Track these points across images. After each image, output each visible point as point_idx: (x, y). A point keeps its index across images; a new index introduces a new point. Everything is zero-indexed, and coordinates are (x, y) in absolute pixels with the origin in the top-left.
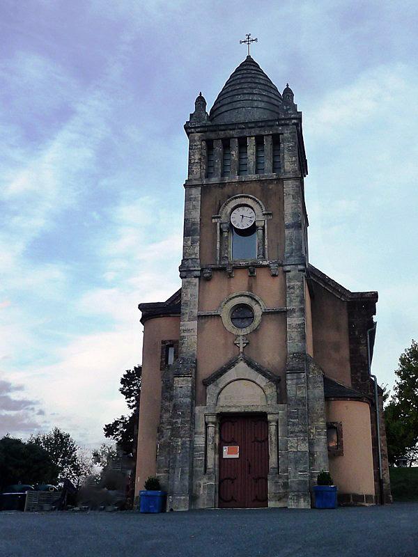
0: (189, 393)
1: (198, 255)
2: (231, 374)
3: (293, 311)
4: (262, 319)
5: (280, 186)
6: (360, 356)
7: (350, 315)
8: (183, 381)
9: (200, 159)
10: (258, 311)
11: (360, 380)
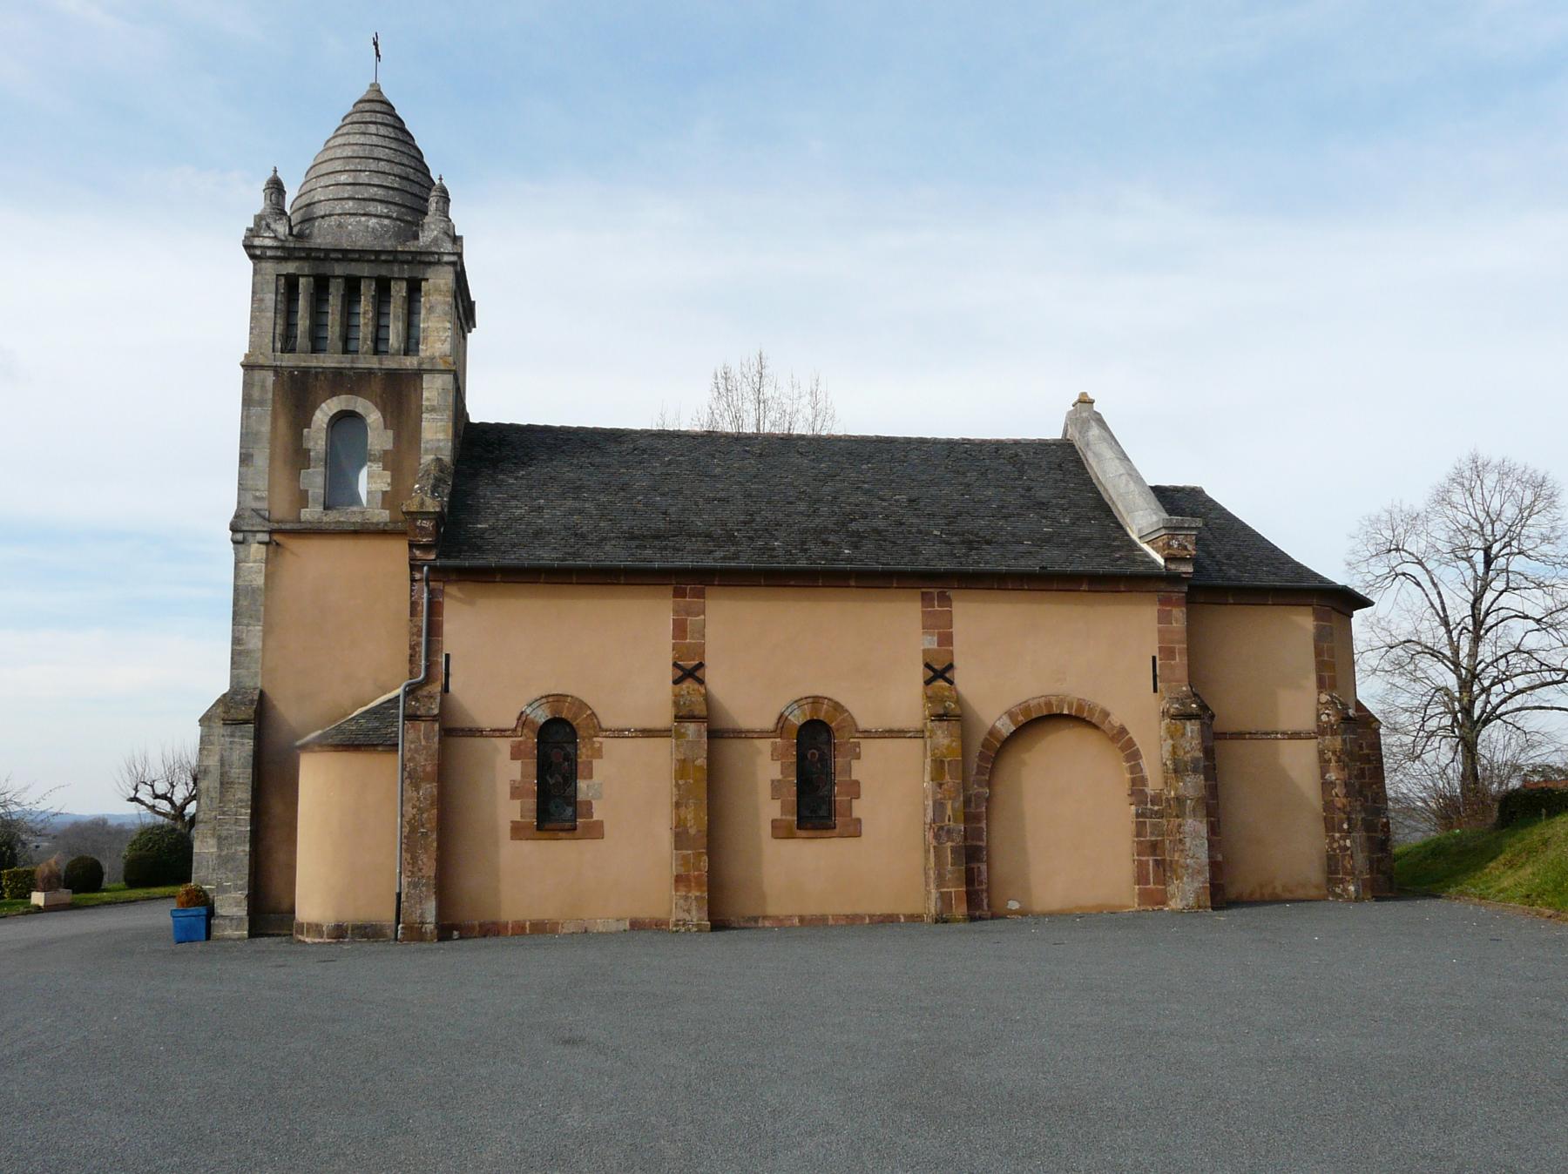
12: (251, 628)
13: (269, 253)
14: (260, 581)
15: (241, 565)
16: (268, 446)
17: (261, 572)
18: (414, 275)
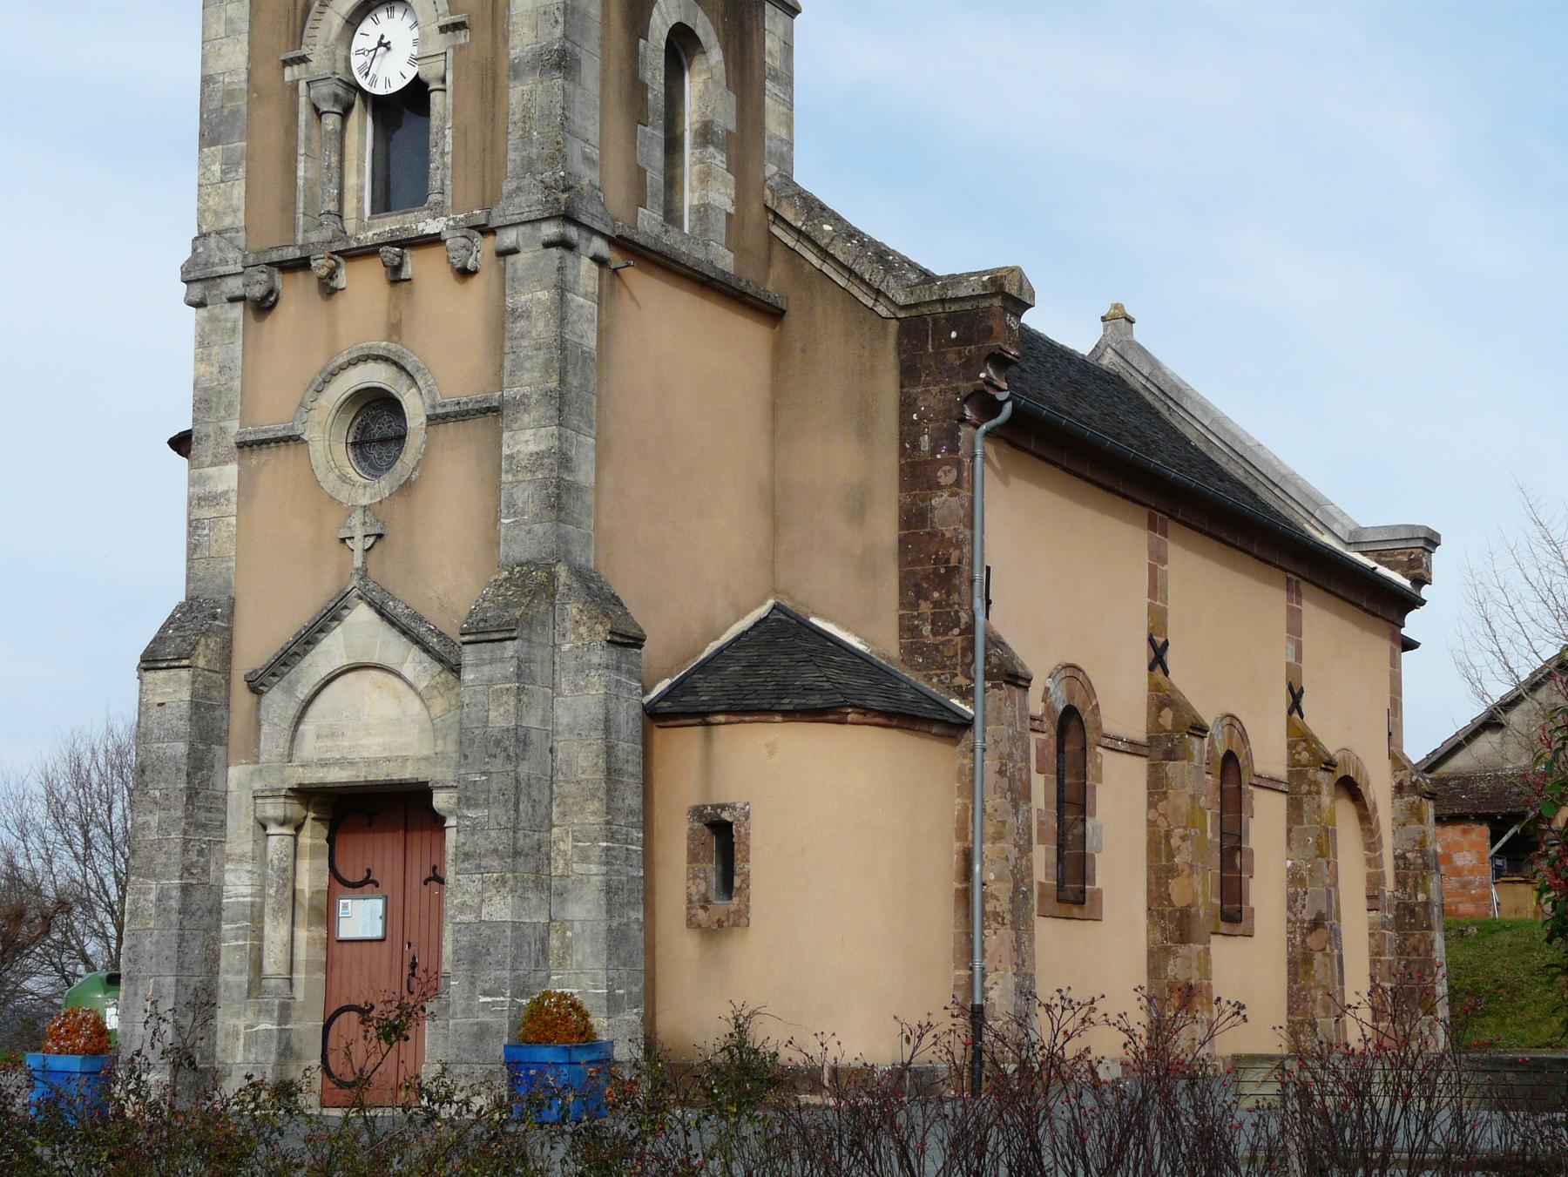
0: (184, 727)
1: (241, 215)
2: (332, 651)
3: (520, 403)
4: (429, 444)
6: (932, 535)
7: (909, 373)
8: (166, 681)
10: (415, 408)
11: (926, 629)
12: (582, 438)
14: (591, 341)
15: (569, 295)
16: (598, 51)
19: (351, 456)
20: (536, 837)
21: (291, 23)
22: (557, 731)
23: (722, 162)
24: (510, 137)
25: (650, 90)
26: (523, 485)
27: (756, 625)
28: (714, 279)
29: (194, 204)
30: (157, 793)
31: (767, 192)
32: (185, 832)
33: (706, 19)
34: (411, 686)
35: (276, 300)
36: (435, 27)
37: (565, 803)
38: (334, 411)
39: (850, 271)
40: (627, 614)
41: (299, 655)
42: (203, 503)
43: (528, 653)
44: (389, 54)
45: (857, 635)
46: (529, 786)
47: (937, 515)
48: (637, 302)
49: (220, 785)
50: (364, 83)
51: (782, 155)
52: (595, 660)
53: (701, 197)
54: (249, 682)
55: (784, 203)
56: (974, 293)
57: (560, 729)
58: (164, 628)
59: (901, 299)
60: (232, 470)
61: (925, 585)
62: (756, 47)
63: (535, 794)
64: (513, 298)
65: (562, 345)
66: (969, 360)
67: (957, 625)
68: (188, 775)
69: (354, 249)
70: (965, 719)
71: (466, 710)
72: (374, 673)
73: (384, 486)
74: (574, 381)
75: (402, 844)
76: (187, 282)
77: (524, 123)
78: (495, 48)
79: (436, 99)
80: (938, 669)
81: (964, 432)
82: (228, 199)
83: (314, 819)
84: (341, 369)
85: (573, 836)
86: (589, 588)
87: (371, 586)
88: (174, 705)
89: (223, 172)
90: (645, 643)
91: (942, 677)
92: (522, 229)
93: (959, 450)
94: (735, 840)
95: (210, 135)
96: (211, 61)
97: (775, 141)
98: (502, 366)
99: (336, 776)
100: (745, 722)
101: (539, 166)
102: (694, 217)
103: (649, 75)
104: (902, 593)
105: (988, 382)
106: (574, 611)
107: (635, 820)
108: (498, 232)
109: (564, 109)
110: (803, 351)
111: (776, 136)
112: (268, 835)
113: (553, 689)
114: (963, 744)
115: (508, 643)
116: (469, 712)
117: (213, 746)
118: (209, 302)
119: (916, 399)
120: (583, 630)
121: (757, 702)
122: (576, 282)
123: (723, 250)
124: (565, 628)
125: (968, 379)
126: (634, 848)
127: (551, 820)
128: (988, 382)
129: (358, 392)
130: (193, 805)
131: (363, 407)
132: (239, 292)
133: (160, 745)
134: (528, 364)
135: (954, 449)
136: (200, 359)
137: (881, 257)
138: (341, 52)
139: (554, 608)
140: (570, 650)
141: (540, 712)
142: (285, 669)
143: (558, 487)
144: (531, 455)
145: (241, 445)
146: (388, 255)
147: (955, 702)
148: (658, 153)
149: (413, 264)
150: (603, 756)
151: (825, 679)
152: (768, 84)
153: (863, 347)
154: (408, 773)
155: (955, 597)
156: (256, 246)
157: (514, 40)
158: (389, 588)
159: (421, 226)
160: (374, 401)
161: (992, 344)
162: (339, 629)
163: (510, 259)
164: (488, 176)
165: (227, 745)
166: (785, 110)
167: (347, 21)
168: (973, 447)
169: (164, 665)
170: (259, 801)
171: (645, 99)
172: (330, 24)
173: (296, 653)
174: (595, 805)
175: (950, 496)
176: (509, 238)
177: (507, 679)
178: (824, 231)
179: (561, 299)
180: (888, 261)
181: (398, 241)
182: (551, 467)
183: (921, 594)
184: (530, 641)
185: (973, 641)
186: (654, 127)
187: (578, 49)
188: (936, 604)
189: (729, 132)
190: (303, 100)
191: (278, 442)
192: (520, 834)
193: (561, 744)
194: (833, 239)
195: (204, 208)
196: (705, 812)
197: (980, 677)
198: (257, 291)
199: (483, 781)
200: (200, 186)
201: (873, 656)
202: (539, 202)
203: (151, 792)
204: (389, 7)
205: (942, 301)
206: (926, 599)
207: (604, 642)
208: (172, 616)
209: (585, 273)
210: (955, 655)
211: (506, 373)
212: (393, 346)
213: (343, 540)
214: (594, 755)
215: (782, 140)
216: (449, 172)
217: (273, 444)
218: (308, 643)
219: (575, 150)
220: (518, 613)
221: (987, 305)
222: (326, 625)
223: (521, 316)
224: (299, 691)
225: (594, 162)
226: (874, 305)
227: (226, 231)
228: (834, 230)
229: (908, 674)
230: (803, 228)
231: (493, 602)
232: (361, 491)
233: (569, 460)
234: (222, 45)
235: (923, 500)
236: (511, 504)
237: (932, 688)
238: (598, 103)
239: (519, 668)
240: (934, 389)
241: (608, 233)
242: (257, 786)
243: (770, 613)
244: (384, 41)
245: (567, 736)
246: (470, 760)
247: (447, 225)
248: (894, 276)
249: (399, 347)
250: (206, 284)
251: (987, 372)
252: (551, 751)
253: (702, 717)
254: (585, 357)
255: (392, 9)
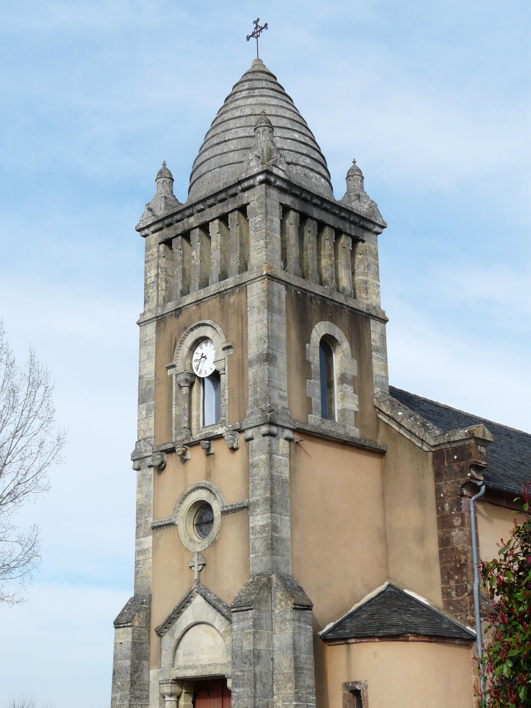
0: (129, 653)
1: (153, 431)
4: (222, 523)
5: (243, 295)
6: (453, 549)
7: (438, 476)
8: (123, 633)
9: (157, 275)
11: (454, 593)
12: (283, 517)
13: (278, 183)
14: (286, 474)
15: (274, 456)
16: (285, 351)
17: (287, 465)
18: (358, 235)
19: (195, 530)
20: (266, 701)
21: (170, 352)
22: (275, 650)
23: (351, 390)
24: (249, 391)
25: (312, 364)
26: (258, 540)
27: (379, 594)
28: (347, 441)
29: (136, 428)
30: (120, 684)
31: (375, 400)
32: (130, 701)
33: (339, 330)
34: (218, 631)
35: (165, 466)
36: (221, 348)
37: (279, 684)
38: (187, 511)
39: (411, 432)
40: (305, 595)
41: (175, 619)
42: (140, 554)
43: (259, 615)
44: (206, 360)
45: (424, 597)
46: (261, 676)
47: (455, 540)
48: (309, 455)
49: (146, 679)
50: (197, 373)
51: (382, 383)
52: (288, 617)
53: (342, 406)
54: (156, 631)
55: (382, 404)
56: (462, 438)
57: (276, 649)
58: (124, 609)
59: (432, 443)
60: (150, 538)
61: (452, 573)
62: (366, 339)
63: (265, 680)
64: (252, 459)
65: (271, 477)
66: (463, 468)
67: (467, 591)
68: (131, 675)
69: (192, 442)
70: (473, 636)
71: (234, 642)
72: (204, 626)
73: (206, 543)
74: (278, 492)
75: (221, 704)
76: (133, 460)
77: (254, 384)
78: (242, 354)
79: (222, 377)
80: (460, 612)
81: (464, 501)
82: (148, 425)
83: (185, 693)
84: (189, 493)
85: (282, 699)
86: (286, 584)
87: (201, 587)
88: (126, 643)
89: (146, 414)
90: (313, 608)
91: (462, 616)
92: (254, 429)
93: (461, 509)
94: (362, 699)
95: (142, 400)
96: (142, 371)
97: (378, 377)
98: (248, 488)
99: (190, 673)
100: (363, 642)
101: (260, 402)
102: (339, 415)
103: (311, 358)
104: (442, 577)
105: (472, 477)
106: (279, 595)
107: (311, 691)
108: (245, 431)
109: (269, 378)
110: (394, 468)
111: (378, 375)
112: (166, 701)
113: (272, 631)
114: (473, 648)
115: (250, 611)
116: (235, 643)
117: (142, 661)
118: (141, 468)
119: (442, 487)
120: (283, 603)
121: (368, 632)
122: (277, 450)
123: (353, 428)
124: (276, 603)
125: (463, 477)
126: (311, 704)
127: (273, 692)
128: (472, 477)
129: (196, 502)
130: (133, 688)
131: (199, 508)
132: (151, 463)
133: (121, 661)
134: (258, 487)
135: (459, 509)
136: (139, 492)
137: (424, 424)
138: (188, 362)
139: (271, 594)
140: (278, 613)
141: (266, 642)
142: (170, 625)
143: (271, 540)
144: (261, 526)
145: (153, 528)
146: (203, 444)
147: (468, 628)
148: (317, 391)
149: (215, 447)
150: (293, 661)
151: (401, 620)
152: (374, 354)
153: (419, 465)
154: (217, 671)
155: (465, 578)
156: (158, 444)
157: (250, 351)
158: (208, 587)
159: (216, 431)
160: (203, 506)
161: (472, 460)
162: (190, 607)
163: (251, 442)
164: (241, 408)
165: (149, 660)
166: (384, 363)
167: (190, 349)
168: (469, 508)
169: (122, 626)
170: (161, 685)
171: (310, 368)
172: (184, 351)
173: (174, 618)
174: (290, 685)
175: (459, 531)
176: (249, 434)
177: (249, 628)
178: (398, 415)
179: (270, 458)
180: (426, 426)
181: (208, 438)
182: (268, 531)
183: (450, 577)
184: (259, 610)
185: (473, 599)
186: (315, 379)
187: (275, 352)
188: (457, 581)
189: (354, 377)
190: (174, 382)
191: (170, 525)
192: (257, 700)
193: (276, 656)
194: (402, 418)
195: (140, 429)
196: (349, 685)
197: (477, 616)
198: (157, 463)
199: (241, 675)
200: (138, 420)
201: (432, 607)
202: (260, 418)
203: (117, 683)
204: (206, 341)
205: (449, 443)
206: (452, 579)
207: (291, 609)
208: (128, 603)
209: (282, 445)
210: (467, 606)
211: (250, 491)
212: (208, 482)
213: (191, 567)
214: (289, 661)
215: (382, 377)
216: (227, 407)
217: (165, 527)
218: (178, 613)
219: (275, 394)
220: (253, 597)
221: (468, 443)
222: (185, 605)
223: (255, 466)
224: (176, 634)
225: (285, 398)
226: (422, 446)
227: (147, 438)
228: (403, 414)
229: (448, 616)
230: (390, 415)
231: (245, 593)
232: (197, 545)
233: (276, 527)
234: (146, 363)
235: (448, 533)
236: (254, 549)
237: (458, 622)
238: (286, 373)
239: (254, 622)
240: (449, 482)
241: (292, 427)
242: (161, 678)
243: (386, 589)
244: (203, 356)
245: (279, 652)
246: (236, 665)
247: (226, 430)
248: (429, 433)
249: (210, 482)
250: (140, 461)
251: (471, 473)
252: (272, 659)
253: (344, 640)
254: (283, 482)
255: (207, 342)
